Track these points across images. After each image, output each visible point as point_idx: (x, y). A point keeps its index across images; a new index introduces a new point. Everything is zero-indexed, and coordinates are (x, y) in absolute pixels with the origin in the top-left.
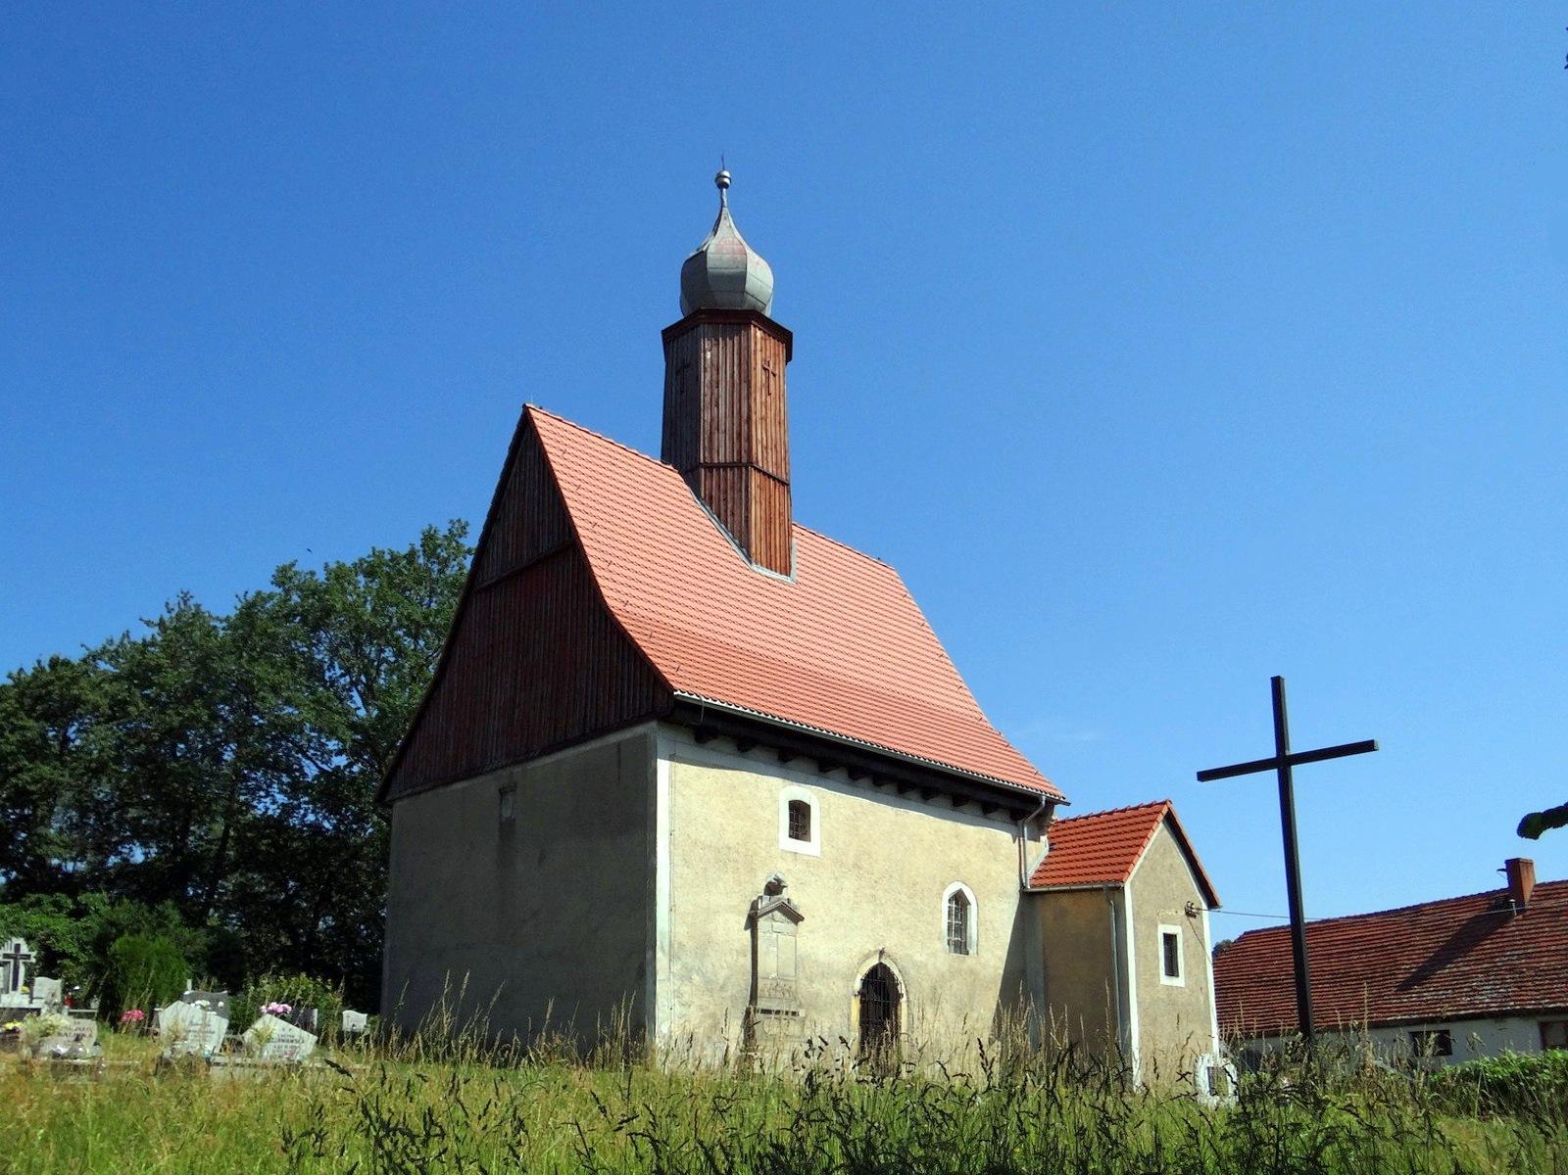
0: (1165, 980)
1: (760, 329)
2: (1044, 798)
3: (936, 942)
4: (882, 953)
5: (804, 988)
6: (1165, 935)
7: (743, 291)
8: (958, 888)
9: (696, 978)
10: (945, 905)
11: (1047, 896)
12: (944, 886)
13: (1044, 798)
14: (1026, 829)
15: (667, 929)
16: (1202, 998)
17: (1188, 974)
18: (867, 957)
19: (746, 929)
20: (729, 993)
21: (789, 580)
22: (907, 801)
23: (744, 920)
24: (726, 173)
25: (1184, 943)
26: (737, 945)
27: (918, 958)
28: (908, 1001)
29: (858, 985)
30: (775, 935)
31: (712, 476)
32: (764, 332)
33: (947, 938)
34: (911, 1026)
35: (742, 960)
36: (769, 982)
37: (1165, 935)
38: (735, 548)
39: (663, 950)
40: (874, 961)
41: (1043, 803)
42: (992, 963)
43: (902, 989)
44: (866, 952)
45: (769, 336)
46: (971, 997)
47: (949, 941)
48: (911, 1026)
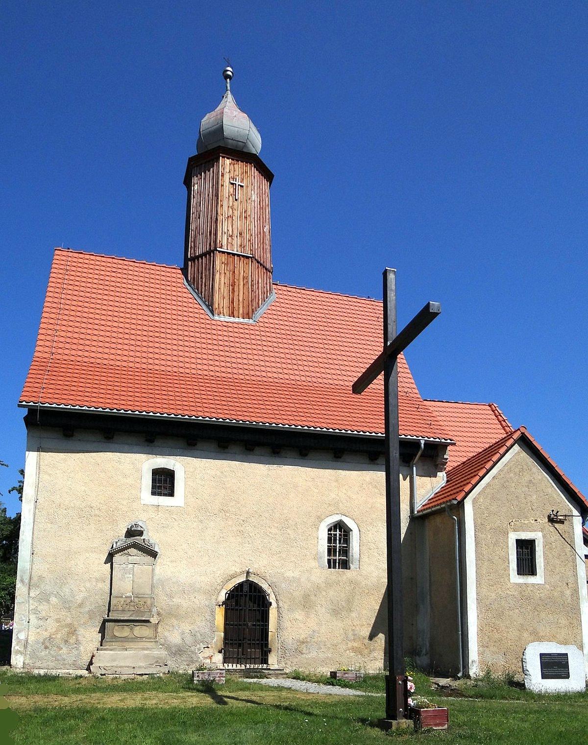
0: (515, 578)
1: (228, 158)
2: (423, 442)
3: (310, 561)
4: (248, 573)
5: (162, 601)
6: (517, 541)
7: (224, 138)
8: (340, 519)
9: (54, 600)
10: (323, 535)
11: (431, 518)
12: (320, 519)
13: (423, 442)
14: (415, 468)
15: (28, 566)
16: (568, 592)
17: (550, 570)
18: (233, 577)
19: (105, 563)
20: (87, 609)
21: (251, 321)
22: (306, 461)
23: (104, 557)
24: (229, 68)
25: (544, 547)
26: (97, 575)
27: (289, 574)
28: (278, 607)
29: (222, 597)
30: (131, 566)
31: (195, 264)
32: (232, 159)
33: (326, 558)
34: (279, 627)
35: (100, 585)
36: (122, 600)
37: (517, 541)
38: (204, 307)
39: (22, 581)
40: (242, 579)
41: (423, 445)
42: (375, 574)
43: (272, 599)
44: (231, 573)
45: (238, 161)
46: (349, 601)
47: (329, 561)
48: (279, 627)
